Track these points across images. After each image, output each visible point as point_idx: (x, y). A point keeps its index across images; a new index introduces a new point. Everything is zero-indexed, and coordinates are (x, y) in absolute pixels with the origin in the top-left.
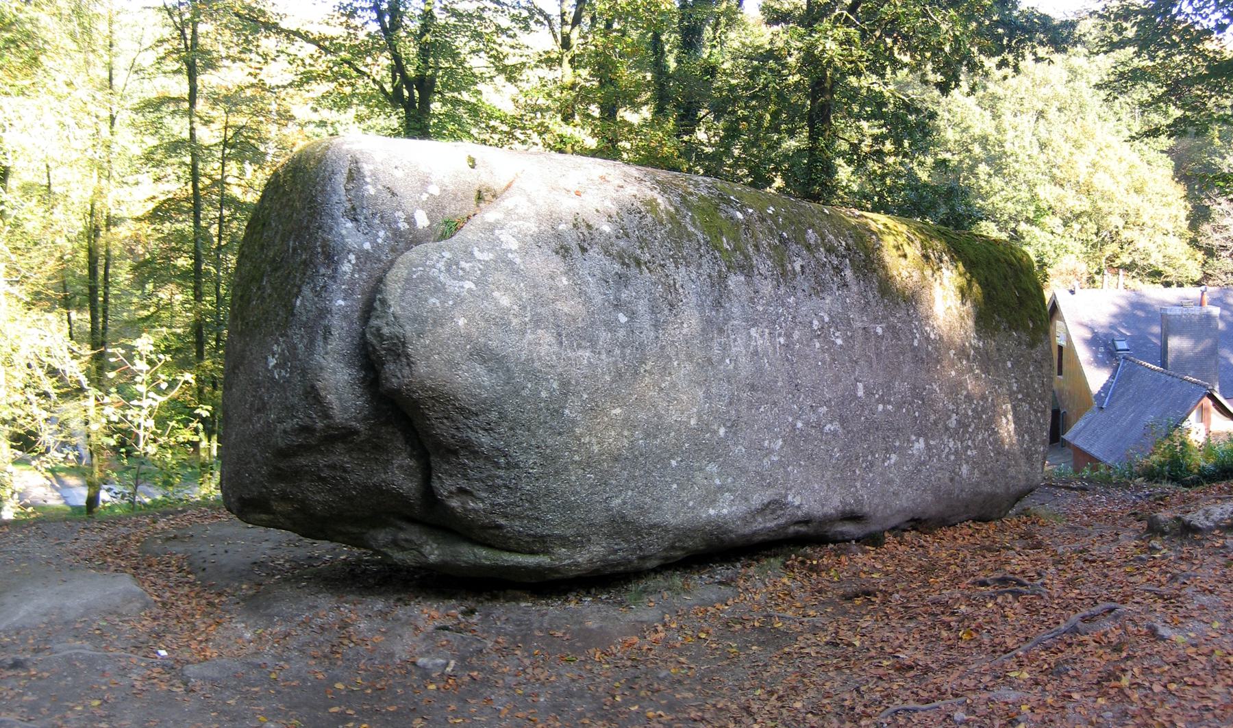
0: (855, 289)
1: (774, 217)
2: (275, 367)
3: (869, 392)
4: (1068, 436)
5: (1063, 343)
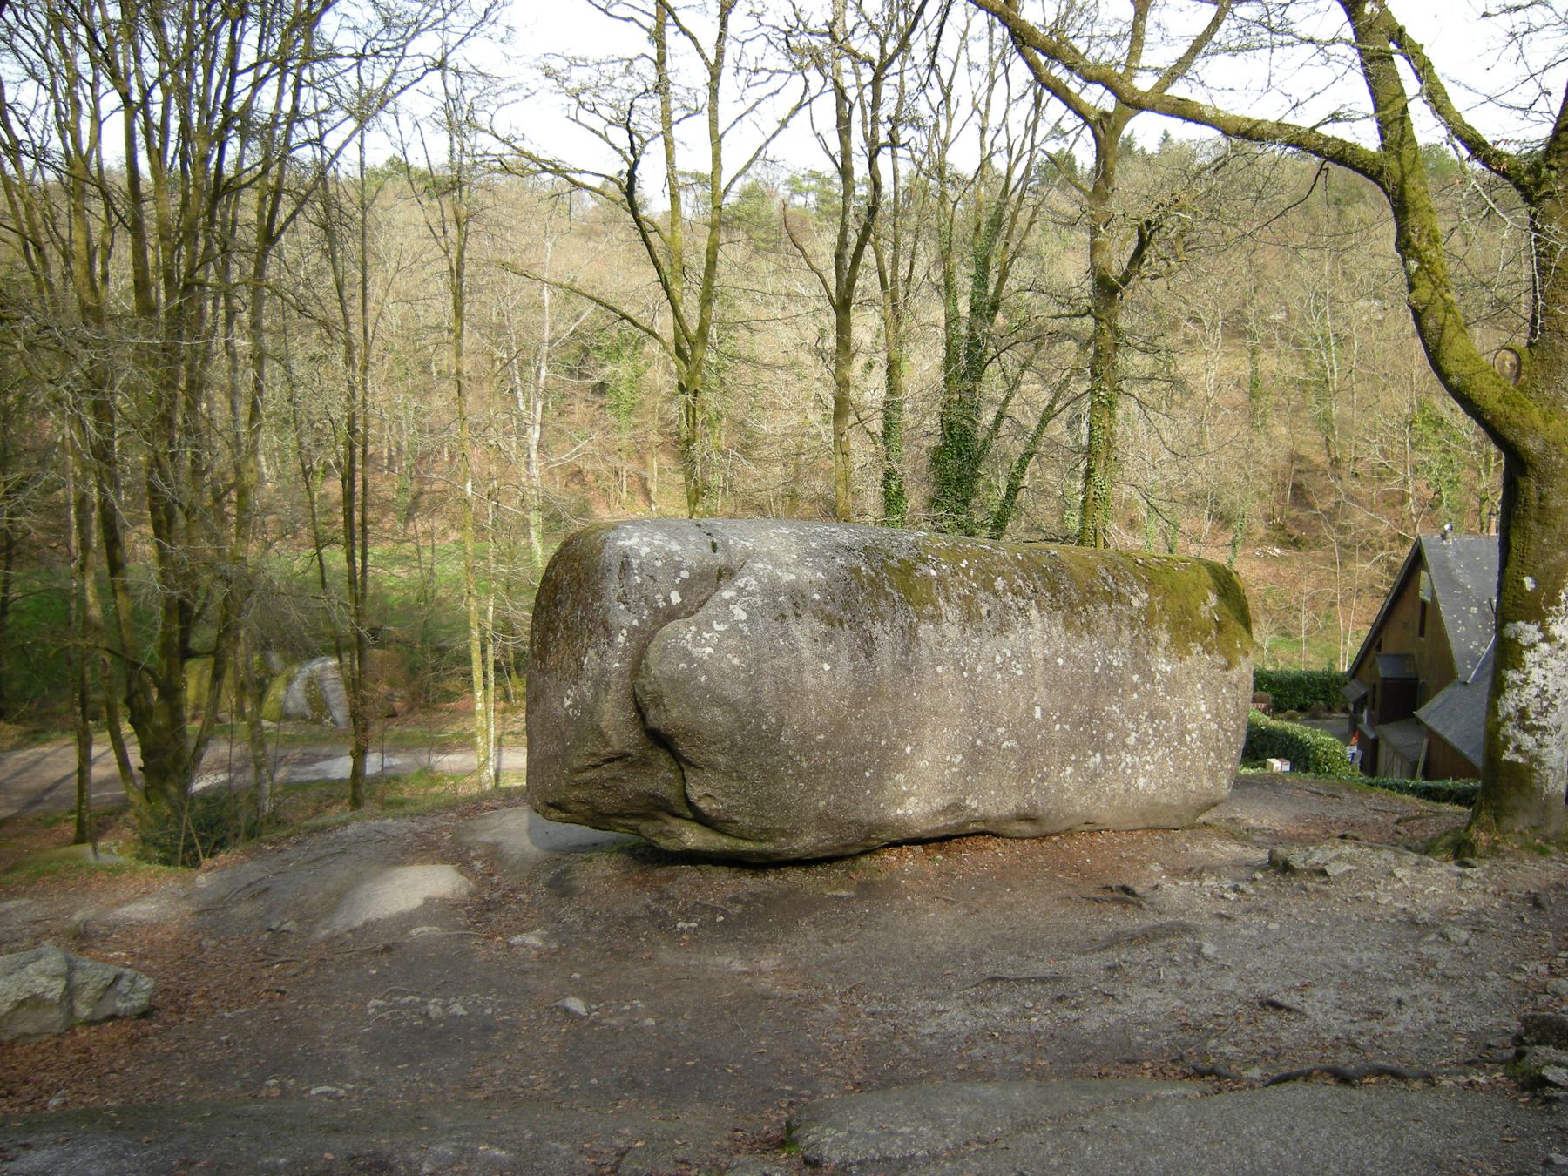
0: (1039, 626)
1: (966, 571)
2: (570, 706)
3: (1045, 713)
4: (1421, 713)
5: (1427, 599)
